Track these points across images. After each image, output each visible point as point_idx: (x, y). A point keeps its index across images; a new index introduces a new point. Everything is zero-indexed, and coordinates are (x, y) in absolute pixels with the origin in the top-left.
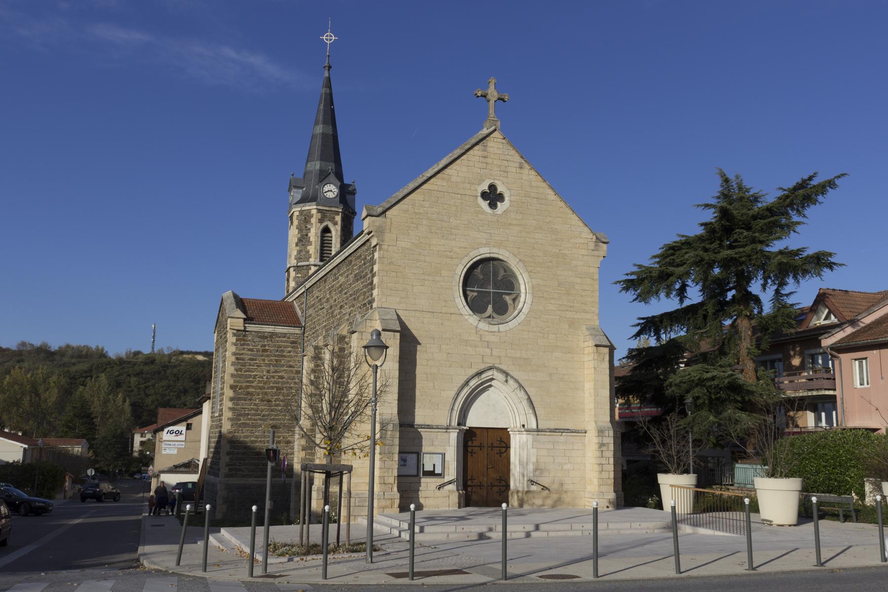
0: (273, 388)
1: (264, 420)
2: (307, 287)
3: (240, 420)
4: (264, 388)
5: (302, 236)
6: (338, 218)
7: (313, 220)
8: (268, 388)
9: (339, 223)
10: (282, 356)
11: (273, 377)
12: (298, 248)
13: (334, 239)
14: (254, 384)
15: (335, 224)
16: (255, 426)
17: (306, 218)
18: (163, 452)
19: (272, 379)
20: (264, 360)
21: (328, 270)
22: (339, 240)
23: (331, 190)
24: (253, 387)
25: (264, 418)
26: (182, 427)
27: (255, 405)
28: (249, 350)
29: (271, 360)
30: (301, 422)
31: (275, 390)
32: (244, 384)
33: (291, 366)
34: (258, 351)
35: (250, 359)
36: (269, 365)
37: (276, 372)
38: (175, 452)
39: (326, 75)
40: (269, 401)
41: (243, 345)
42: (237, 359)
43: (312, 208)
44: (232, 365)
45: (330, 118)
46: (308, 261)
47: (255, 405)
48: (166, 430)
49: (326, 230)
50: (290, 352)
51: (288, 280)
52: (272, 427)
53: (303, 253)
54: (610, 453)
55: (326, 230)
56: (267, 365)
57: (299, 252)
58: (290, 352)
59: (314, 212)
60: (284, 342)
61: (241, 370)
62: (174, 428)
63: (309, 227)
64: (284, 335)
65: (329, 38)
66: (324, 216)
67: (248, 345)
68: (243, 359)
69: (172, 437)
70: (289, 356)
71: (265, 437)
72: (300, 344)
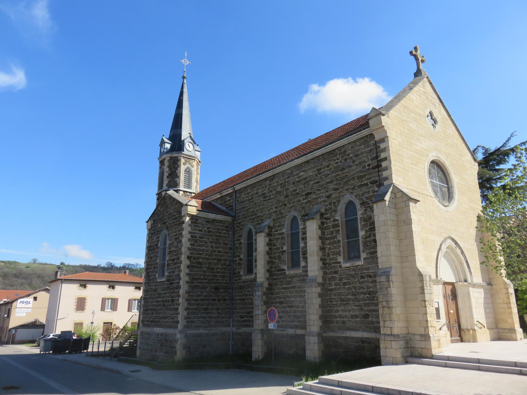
0: (214, 259)
3: (193, 283)
5: (172, 172)
8: (212, 259)
11: (215, 251)
12: (169, 179)
18: (17, 315)
20: (209, 239)
24: (202, 258)
26: (30, 299)
28: (200, 230)
29: (213, 239)
32: (196, 256)
34: (205, 231)
36: (211, 242)
38: (24, 315)
40: (212, 269)
42: (192, 236)
44: (188, 241)
47: (204, 271)
48: (19, 301)
50: (225, 234)
56: (211, 242)
57: (169, 182)
58: (225, 234)
62: (25, 300)
64: (221, 221)
65: (186, 62)
68: (196, 237)
69: (23, 305)
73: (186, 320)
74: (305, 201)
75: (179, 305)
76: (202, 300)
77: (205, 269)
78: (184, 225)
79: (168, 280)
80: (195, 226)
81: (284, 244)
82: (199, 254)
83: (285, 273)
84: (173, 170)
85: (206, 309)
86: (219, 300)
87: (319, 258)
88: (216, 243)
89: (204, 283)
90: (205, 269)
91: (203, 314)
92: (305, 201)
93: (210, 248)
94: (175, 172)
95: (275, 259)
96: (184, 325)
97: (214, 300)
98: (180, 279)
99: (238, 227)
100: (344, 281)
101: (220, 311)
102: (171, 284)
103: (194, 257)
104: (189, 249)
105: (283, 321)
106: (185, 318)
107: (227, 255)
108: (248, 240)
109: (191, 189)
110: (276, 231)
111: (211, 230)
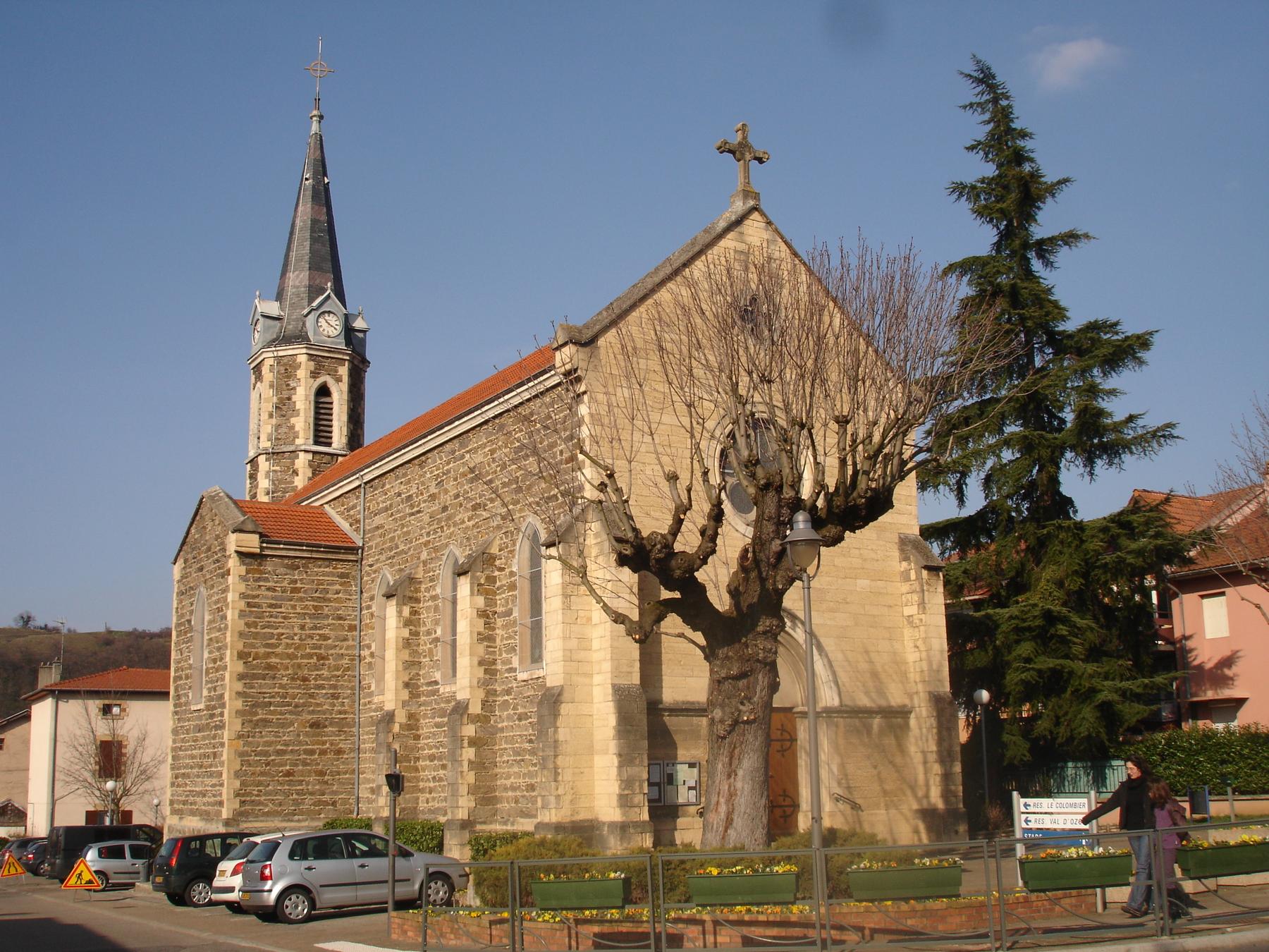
0: (310, 656)
1: (298, 714)
2: (367, 478)
3: (256, 714)
4: (296, 657)
5: (281, 400)
6: (344, 371)
7: (302, 373)
8: (302, 657)
9: (345, 378)
10: (325, 600)
13: (336, 407)
14: (279, 650)
15: (339, 380)
16: (283, 726)
17: (287, 370)
19: (309, 641)
20: (294, 607)
21: (432, 445)
22: (345, 408)
23: (330, 328)
24: (277, 655)
25: (297, 710)
27: (282, 686)
28: (268, 589)
30: (1028, 746)
31: (314, 660)
32: (262, 650)
33: (340, 618)
35: (271, 606)
37: (315, 628)
39: (315, 127)
40: (305, 679)
41: (259, 579)
42: (249, 605)
43: (300, 353)
46: (293, 443)
47: (282, 686)
49: (323, 391)
50: (338, 593)
51: (253, 477)
52: (311, 726)
53: (284, 430)
55: (323, 391)
59: (302, 359)
60: (328, 574)
61: (255, 625)
63: (292, 384)
66: (320, 363)
67: (266, 580)
68: (259, 606)
71: (300, 743)
72: (354, 578)
73: (238, 800)
75: (222, 764)
76: (279, 753)
77: (285, 680)
78: (230, 579)
79: (208, 708)
81: (437, 623)
82: (268, 646)
83: (438, 690)
86: (323, 752)
88: (312, 616)
90: (285, 680)
93: (296, 630)
94: (289, 399)
97: (312, 752)
98: (223, 706)
99: (369, 575)
100: (520, 710)
103: (257, 654)
104: (241, 634)
105: (434, 799)
106: (237, 795)
107: (345, 644)
108: (532, 567)
110: (427, 590)
111: (299, 585)
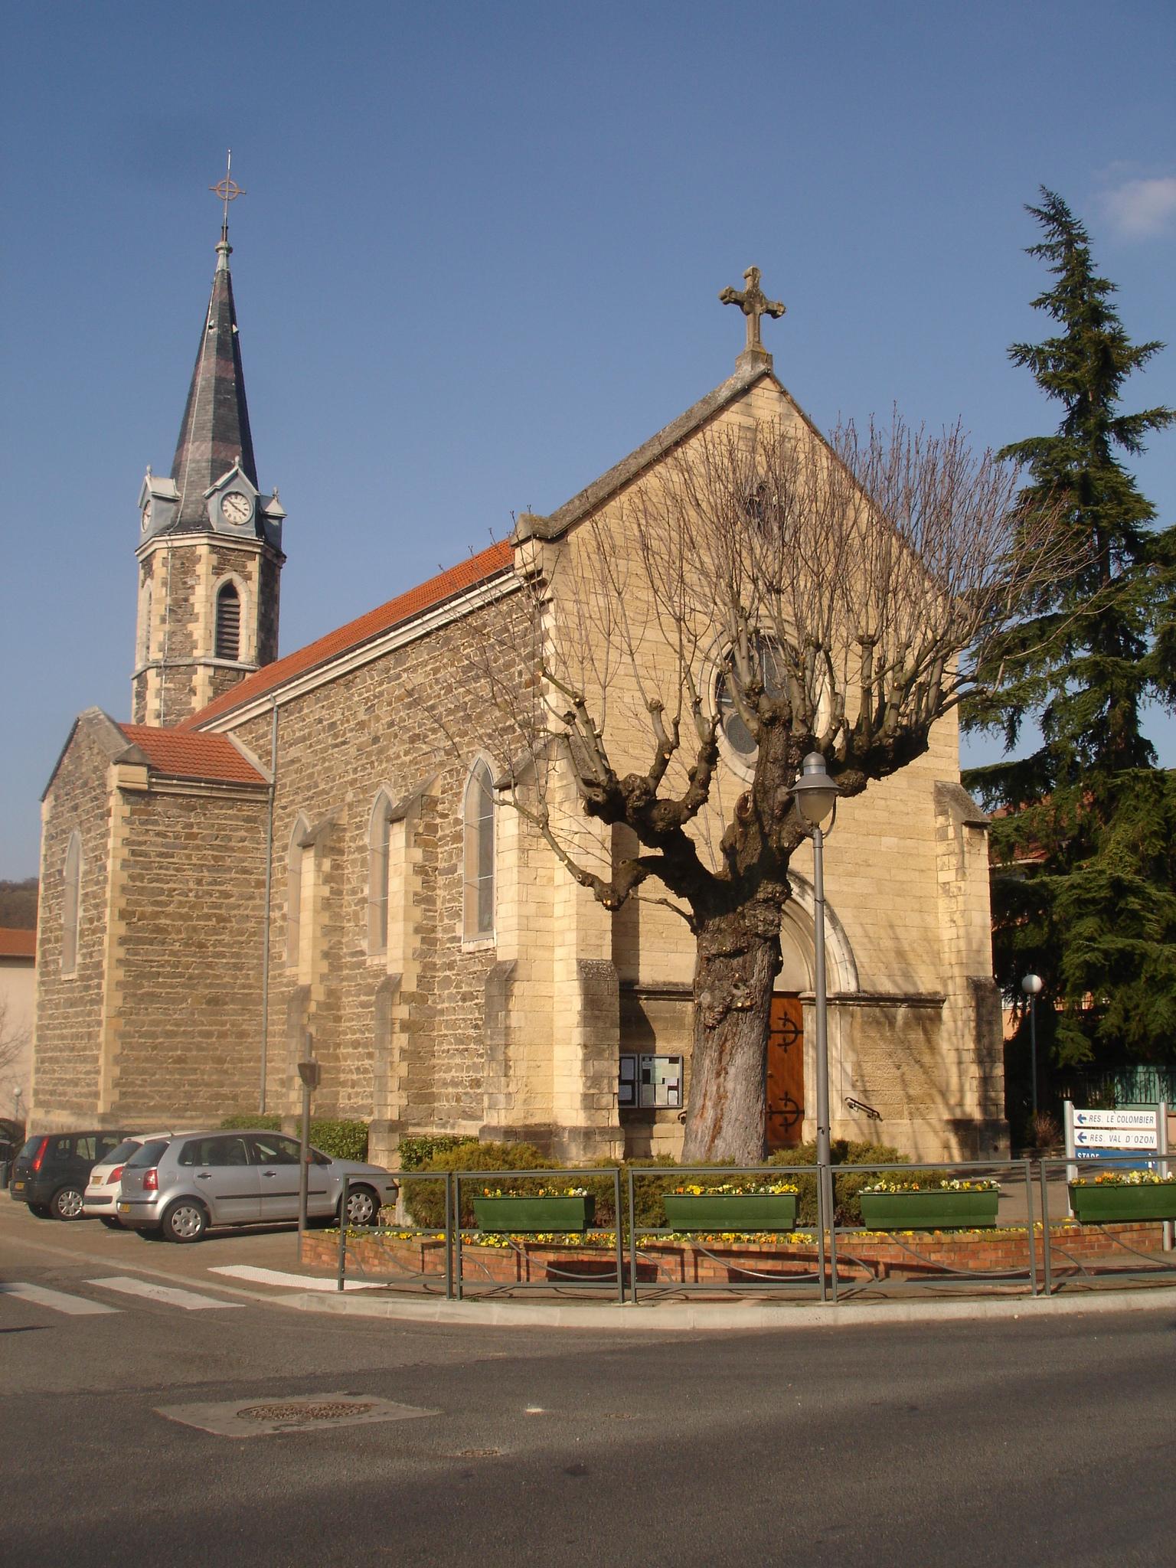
0: (208, 917)
2: (281, 700)
3: (141, 986)
4: (191, 918)
6: (254, 567)
7: (202, 569)
8: (199, 918)
9: (256, 576)
12: (167, 627)
14: (170, 909)
15: (247, 578)
16: (174, 1001)
17: (184, 563)
20: (189, 857)
22: (255, 613)
24: (167, 915)
28: (158, 834)
29: (204, 858)
31: (213, 922)
32: (150, 909)
33: (245, 871)
35: (161, 855)
37: (215, 883)
39: (221, 263)
40: (201, 946)
42: (133, 853)
43: (200, 544)
45: (229, 349)
47: (173, 953)
49: (228, 592)
50: (243, 840)
52: (209, 1002)
53: (179, 638)
54: (418, 1319)
55: (228, 592)
58: (243, 840)
59: (203, 551)
61: (141, 877)
63: (190, 582)
67: (156, 823)
70: (242, 849)
71: (194, 1023)
72: (263, 823)
74: (408, 758)
76: (169, 1034)
77: (177, 946)
78: (111, 821)
79: (82, 978)
80: (142, 823)
84: (181, 595)
85: (180, 1060)
86: (223, 1035)
87: (411, 927)
88: (210, 869)
89: (172, 986)
91: (171, 1073)
92: (408, 758)
93: (192, 885)
94: (186, 600)
95: (349, 921)
96: (113, 1103)
97: (208, 1034)
98: (101, 976)
99: (281, 819)
101: (226, 1066)
102: (87, 988)
104: (124, 889)
107: (251, 903)
108: (482, 814)
109: (235, 657)
111: (195, 830)
